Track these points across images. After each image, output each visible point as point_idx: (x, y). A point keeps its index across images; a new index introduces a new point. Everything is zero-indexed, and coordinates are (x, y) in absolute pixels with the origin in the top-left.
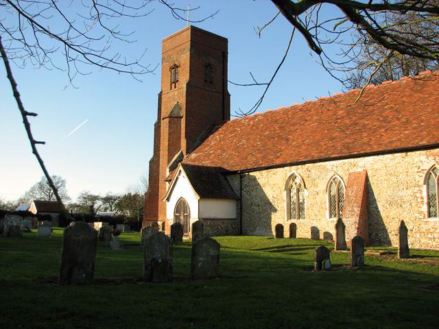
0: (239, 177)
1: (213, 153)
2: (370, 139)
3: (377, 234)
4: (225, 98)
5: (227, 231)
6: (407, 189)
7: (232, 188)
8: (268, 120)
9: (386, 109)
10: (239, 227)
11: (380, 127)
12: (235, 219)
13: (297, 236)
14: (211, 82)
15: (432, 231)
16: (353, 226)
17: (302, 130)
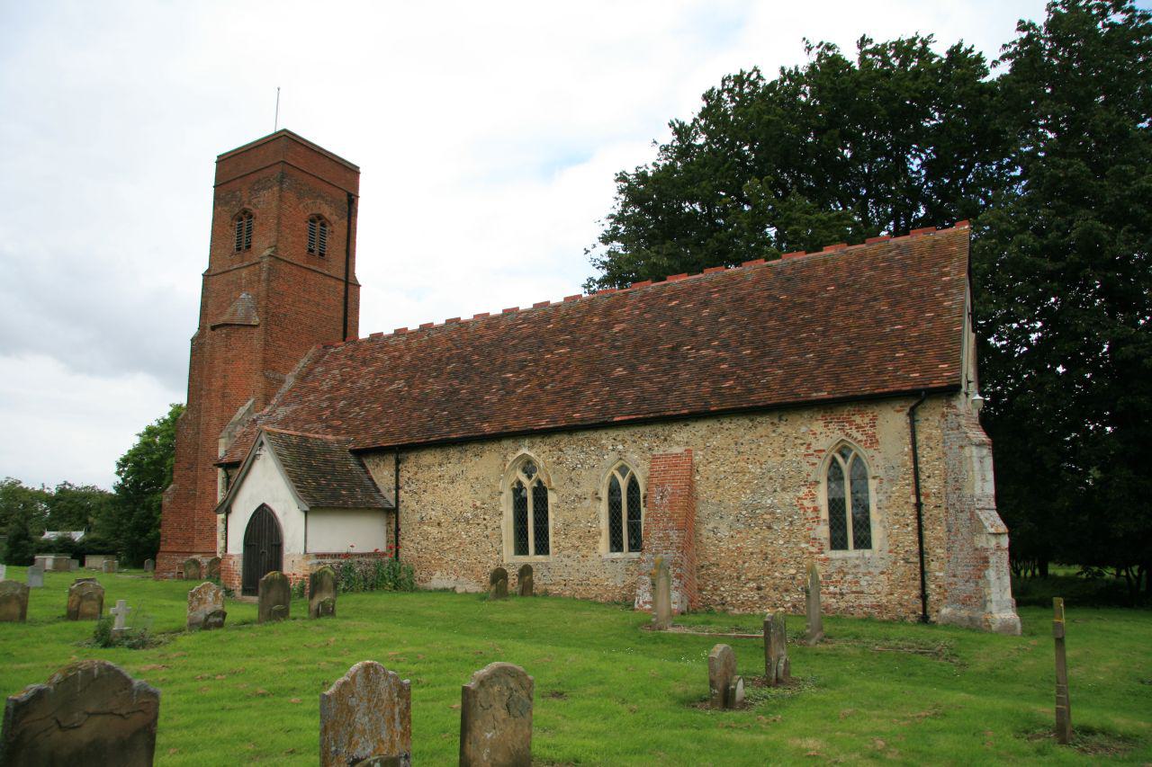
0: (394, 462)
3: (715, 589)
4: (350, 288)
13: (364, 333)
14: (322, 255)
15: (836, 577)
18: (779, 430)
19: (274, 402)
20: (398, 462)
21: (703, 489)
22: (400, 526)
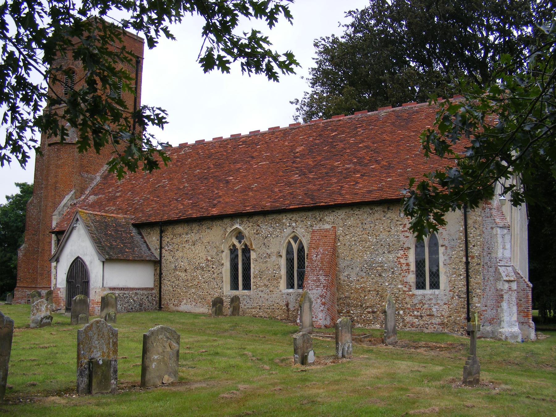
1: (120, 196)
2: (342, 187)
5: (141, 305)
6: (389, 252)
7: (147, 245)
8: (198, 154)
9: (361, 147)
10: (157, 299)
11: (356, 171)
12: (152, 289)
15: (419, 306)
16: (319, 301)
17: (248, 170)
18: (388, 216)
19: (87, 192)
20: (162, 232)
21: (341, 251)
22: (162, 272)
